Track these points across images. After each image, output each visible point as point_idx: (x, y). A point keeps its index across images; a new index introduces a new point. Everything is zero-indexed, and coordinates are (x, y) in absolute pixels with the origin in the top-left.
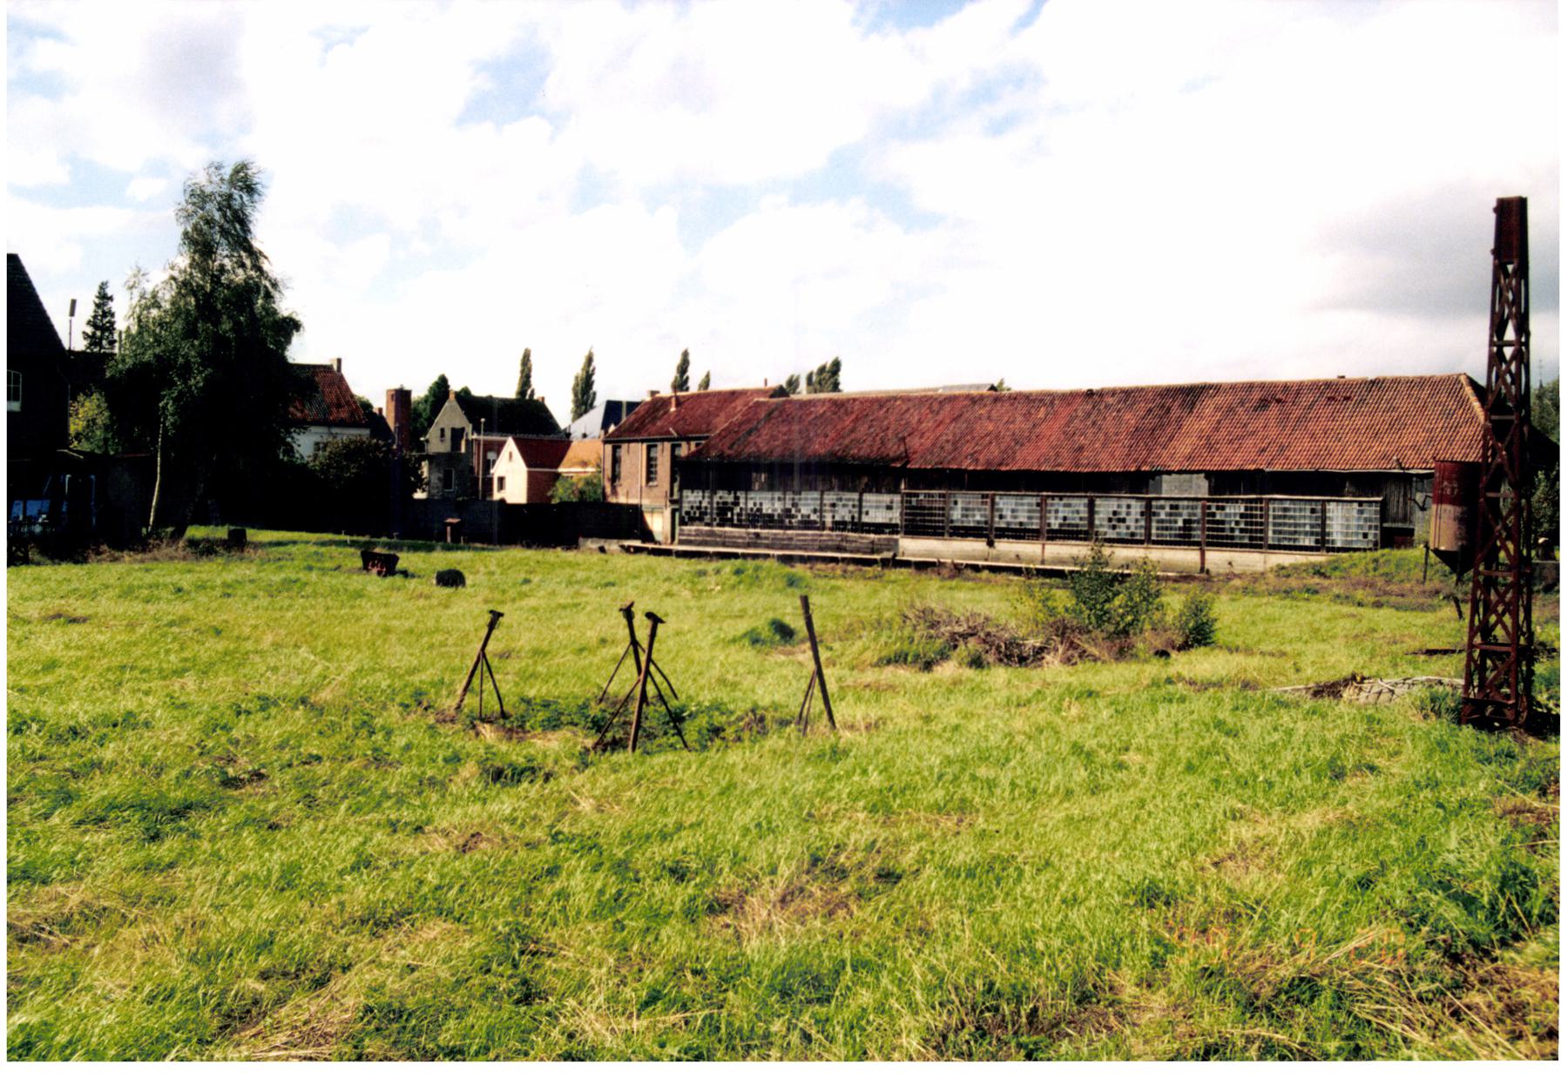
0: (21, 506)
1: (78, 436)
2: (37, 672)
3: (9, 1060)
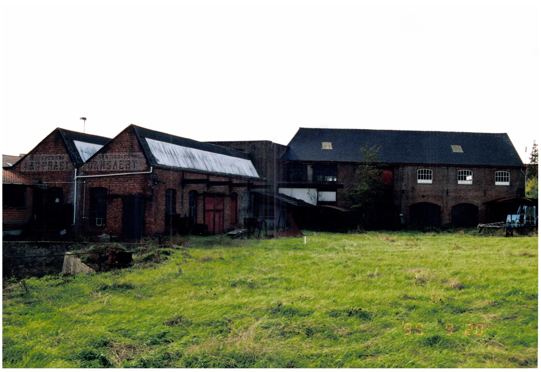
0: (225, 227)
1: (528, 193)
2: (519, 274)
3: (4, 366)
